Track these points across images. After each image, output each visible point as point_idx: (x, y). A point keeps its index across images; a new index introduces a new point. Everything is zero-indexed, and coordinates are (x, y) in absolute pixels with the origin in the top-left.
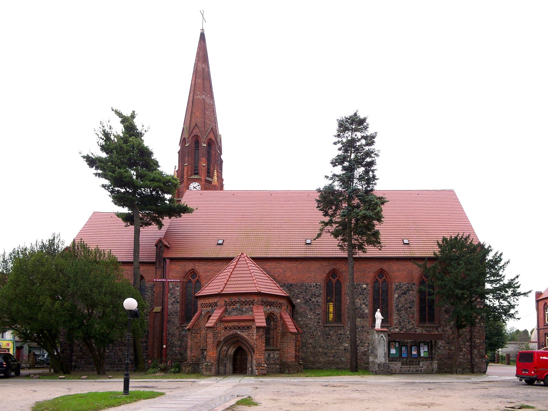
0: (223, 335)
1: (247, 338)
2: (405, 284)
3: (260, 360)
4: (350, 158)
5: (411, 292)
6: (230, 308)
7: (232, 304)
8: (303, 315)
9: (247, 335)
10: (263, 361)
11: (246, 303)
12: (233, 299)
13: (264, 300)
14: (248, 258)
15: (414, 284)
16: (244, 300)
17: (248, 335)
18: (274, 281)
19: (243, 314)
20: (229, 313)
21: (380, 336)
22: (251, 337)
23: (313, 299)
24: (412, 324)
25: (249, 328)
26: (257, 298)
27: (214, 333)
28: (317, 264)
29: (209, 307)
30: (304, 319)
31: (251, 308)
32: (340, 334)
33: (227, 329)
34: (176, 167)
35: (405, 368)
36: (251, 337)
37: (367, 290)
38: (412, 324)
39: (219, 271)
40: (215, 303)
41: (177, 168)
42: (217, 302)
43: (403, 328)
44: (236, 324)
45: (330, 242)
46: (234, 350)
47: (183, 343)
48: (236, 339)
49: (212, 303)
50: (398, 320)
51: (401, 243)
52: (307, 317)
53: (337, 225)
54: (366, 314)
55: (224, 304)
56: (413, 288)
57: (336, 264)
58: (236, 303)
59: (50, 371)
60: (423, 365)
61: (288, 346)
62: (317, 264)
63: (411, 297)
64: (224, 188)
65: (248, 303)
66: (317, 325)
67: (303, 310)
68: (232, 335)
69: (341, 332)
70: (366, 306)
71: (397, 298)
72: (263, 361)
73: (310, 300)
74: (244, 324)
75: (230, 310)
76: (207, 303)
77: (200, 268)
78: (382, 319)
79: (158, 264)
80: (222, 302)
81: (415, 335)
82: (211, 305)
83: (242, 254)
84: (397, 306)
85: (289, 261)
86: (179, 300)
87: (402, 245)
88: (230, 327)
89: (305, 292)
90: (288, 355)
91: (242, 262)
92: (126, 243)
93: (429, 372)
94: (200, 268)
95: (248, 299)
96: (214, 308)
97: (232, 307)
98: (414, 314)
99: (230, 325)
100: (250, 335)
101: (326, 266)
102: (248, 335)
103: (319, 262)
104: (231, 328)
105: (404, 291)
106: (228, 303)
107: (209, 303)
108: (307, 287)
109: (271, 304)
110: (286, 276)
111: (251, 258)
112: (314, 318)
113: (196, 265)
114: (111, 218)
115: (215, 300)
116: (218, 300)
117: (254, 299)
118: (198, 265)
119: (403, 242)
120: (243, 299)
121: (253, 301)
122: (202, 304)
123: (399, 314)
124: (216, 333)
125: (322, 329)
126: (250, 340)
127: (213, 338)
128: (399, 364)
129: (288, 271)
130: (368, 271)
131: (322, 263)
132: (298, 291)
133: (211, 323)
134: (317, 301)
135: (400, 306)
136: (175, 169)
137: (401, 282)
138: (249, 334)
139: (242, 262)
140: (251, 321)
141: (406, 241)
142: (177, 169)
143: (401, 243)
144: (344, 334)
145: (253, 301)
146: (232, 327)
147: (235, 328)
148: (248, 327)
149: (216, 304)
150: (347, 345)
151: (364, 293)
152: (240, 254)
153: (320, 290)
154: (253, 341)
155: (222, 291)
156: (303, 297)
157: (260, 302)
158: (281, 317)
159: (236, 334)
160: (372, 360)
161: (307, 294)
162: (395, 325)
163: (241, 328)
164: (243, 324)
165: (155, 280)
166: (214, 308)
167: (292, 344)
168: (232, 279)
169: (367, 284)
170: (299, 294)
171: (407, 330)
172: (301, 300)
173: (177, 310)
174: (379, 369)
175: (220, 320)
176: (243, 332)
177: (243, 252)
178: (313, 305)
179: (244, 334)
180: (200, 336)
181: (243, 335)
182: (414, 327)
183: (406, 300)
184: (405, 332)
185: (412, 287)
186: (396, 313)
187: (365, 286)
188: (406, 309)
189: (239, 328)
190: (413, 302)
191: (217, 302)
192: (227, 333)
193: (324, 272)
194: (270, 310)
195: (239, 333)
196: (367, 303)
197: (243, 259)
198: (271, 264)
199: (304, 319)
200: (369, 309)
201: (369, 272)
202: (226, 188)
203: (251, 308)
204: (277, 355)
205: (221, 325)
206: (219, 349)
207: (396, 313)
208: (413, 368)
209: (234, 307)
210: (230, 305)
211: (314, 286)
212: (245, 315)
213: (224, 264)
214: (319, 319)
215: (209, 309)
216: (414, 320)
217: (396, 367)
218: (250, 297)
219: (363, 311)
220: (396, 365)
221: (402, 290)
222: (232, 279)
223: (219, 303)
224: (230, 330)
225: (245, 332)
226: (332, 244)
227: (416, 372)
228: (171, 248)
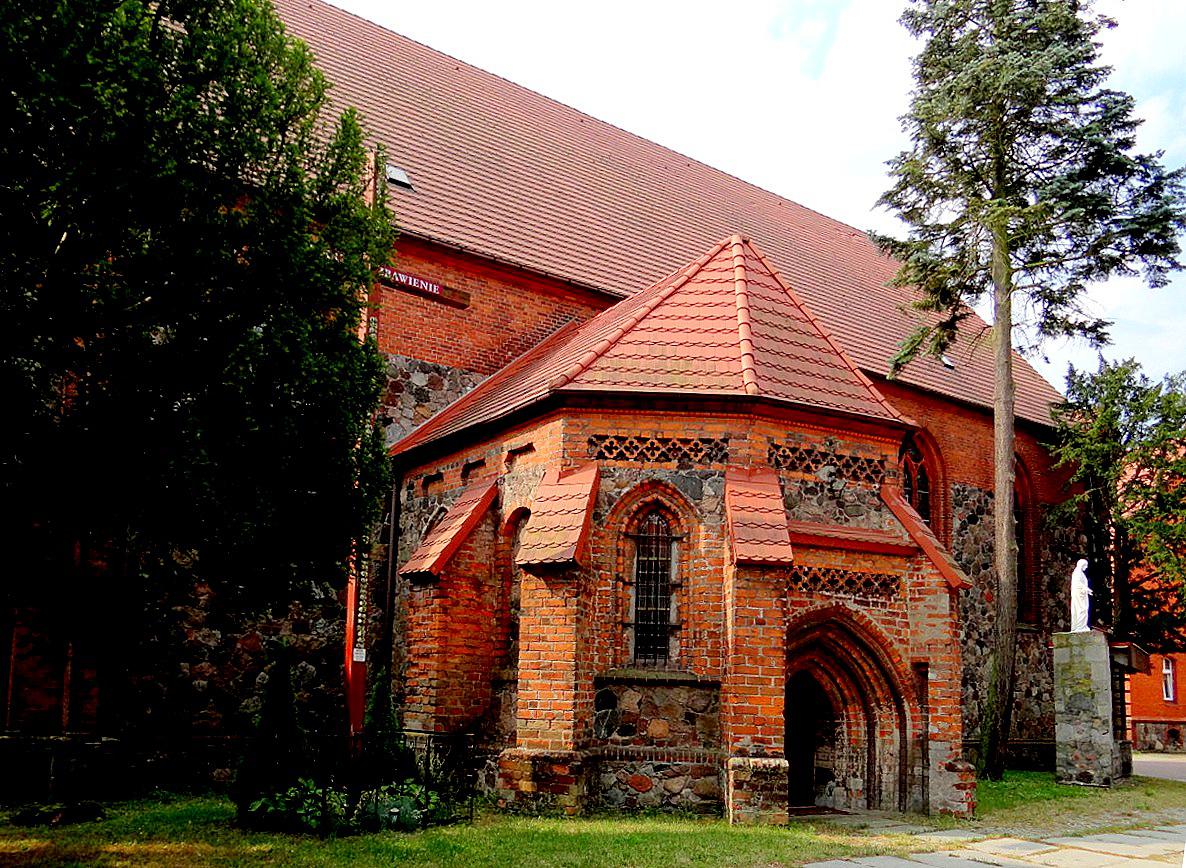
1: (885, 633)
9: (884, 622)
11: (848, 468)
16: (847, 453)
17: (889, 622)
19: (847, 520)
22: (899, 633)
33: (800, 584)
36: (899, 633)
42: (725, 440)
44: (837, 561)
47: (236, 640)
53: (1079, 194)
58: (817, 462)
59: (1128, 679)
68: (823, 613)
74: (869, 565)
76: (642, 440)
80: (762, 447)
88: (811, 575)
95: (863, 448)
96: (697, 468)
97: (799, 475)
102: (889, 622)
104: (815, 579)
105: (972, 511)
120: (844, 447)
121: (881, 463)
126: (896, 646)
140: (895, 555)
146: (820, 575)
147: (833, 582)
148: (885, 585)
155: (569, 380)
159: (840, 611)
163: (860, 584)
164: (863, 566)
166: (697, 468)
176: (868, 604)
179: (874, 616)
189: (850, 583)
192: (801, 604)
195: (852, 606)
209: (807, 476)
210: (793, 467)
212: (852, 523)
215: (665, 472)
218: (870, 444)
223: (739, 449)
224: (812, 586)
225: (875, 604)
226: (419, 223)
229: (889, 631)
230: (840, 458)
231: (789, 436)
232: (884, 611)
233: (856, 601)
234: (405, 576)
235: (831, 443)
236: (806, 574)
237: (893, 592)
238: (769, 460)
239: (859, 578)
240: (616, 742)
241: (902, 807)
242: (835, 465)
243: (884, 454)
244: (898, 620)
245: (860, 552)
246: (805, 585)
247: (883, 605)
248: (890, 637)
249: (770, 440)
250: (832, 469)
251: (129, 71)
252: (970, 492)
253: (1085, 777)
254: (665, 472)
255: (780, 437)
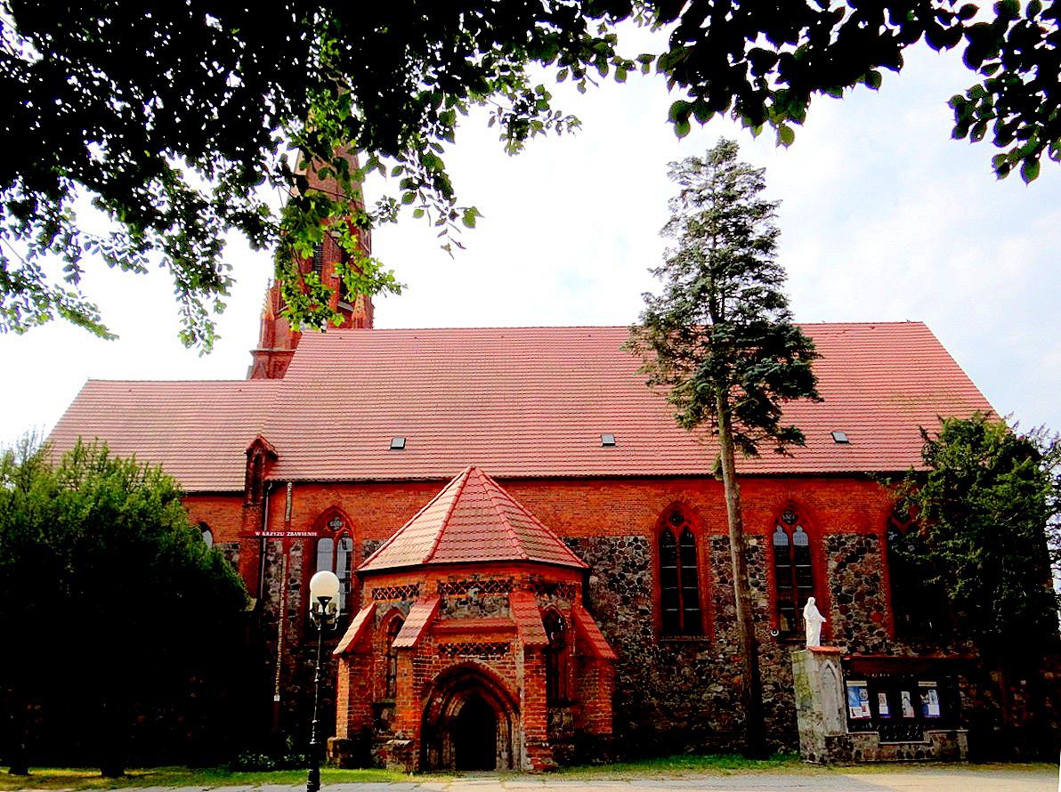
0: (434, 667)
1: (499, 674)
2: (853, 537)
3: (536, 731)
4: (89, 175)
5: (868, 556)
6: (451, 601)
7: (457, 589)
8: (606, 614)
9: (498, 668)
10: (542, 733)
11: (491, 587)
12: (461, 578)
13: (536, 579)
14: (486, 478)
15: (874, 537)
16: (487, 580)
18: (550, 532)
19: (486, 615)
20: (449, 612)
21: (825, 665)
22: (509, 673)
23: (628, 576)
24: (880, 634)
25: (502, 649)
26: (519, 574)
27: (416, 661)
28: (634, 493)
29: (397, 597)
30: (609, 625)
31: (504, 599)
32: (701, 662)
34: (270, 280)
35: (892, 747)
37: (760, 551)
38: (880, 634)
39: (414, 510)
40: (411, 586)
41: (272, 285)
42: (418, 585)
43: (856, 644)
44: (469, 639)
45: (578, 428)
46: (461, 707)
48: (468, 676)
49: (404, 587)
50: (843, 624)
51: (829, 441)
52: (617, 619)
54: (761, 610)
55: (436, 589)
56: (872, 546)
57: (681, 491)
58: (468, 587)
60: (932, 740)
61: (595, 693)
62: (634, 491)
63: (870, 568)
64: (374, 324)
65: (497, 586)
66: (642, 640)
67: (606, 601)
69: (703, 656)
70: (761, 589)
71: (836, 571)
72: (542, 733)
73: (623, 577)
74: (489, 638)
75: (451, 604)
76: (390, 589)
77: (353, 505)
78: (823, 623)
79: (250, 496)
81: (889, 662)
82: (400, 593)
83: (473, 469)
84: (838, 588)
85: (566, 486)
86: (298, 582)
87: (832, 446)
89: (610, 559)
90: (598, 717)
91: (475, 489)
92: (377, 466)
93: (947, 758)
94: (353, 505)
97: (456, 596)
98: (881, 608)
99: (455, 641)
100: (505, 668)
101: (657, 495)
102: (502, 668)
103: (638, 488)
105: (851, 552)
106: (447, 588)
107: (397, 588)
108: (612, 545)
109: (550, 589)
110: (562, 521)
111: (495, 478)
112: (635, 622)
113: (344, 496)
114: (130, 393)
115: (414, 580)
116: (422, 580)
117: (513, 578)
118: (348, 496)
119: (834, 438)
120: (483, 577)
121: (510, 581)
122: (376, 590)
123: (844, 611)
124: (421, 661)
125: (655, 649)
126: (506, 680)
127: (415, 675)
128: (875, 738)
129: (565, 508)
130: (758, 506)
131: (648, 488)
132: (593, 555)
133: (404, 640)
134: (640, 580)
135: (844, 589)
136: (269, 285)
137: (840, 533)
138: (503, 663)
139: (475, 489)
140: (506, 632)
141: (840, 437)
142: (272, 286)
143: (829, 441)
144: (710, 662)
145: (510, 581)
149: (415, 591)
150: (720, 688)
151: (754, 558)
152: (467, 470)
153: (644, 553)
154: (514, 682)
156: (606, 571)
157: (527, 582)
158: (574, 619)
159: (471, 663)
160: (807, 727)
161: (614, 564)
162: (838, 637)
164: (487, 639)
165: (257, 534)
166: (408, 599)
167: (604, 689)
168: (453, 529)
169: (758, 538)
170: (594, 564)
171: (867, 648)
172: (600, 578)
173: (295, 606)
174: (830, 750)
175: (430, 629)
176: (487, 659)
177: (477, 465)
178: (631, 590)
179: (491, 665)
180: (372, 671)
181: (487, 666)
182: (884, 640)
183: (857, 575)
184: (863, 653)
185: (868, 543)
186: (836, 608)
187: (753, 542)
188: (860, 597)
190: (876, 578)
191: (418, 585)
192: (448, 663)
193: (655, 511)
194: (549, 604)
195: (477, 661)
196: (762, 584)
197: (476, 482)
198: (523, 494)
199: (609, 625)
200: (768, 598)
201: (762, 508)
202: (377, 324)
203: (504, 599)
204: (568, 718)
205: (430, 640)
206: (426, 700)
207: (836, 608)
208: (907, 747)
209: (460, 596)
210: (451, 593)
211: (630, 544)
212: (489, 616)
213: (411, 493)
214: (647, 623)
215: (397, 603)
216: (884, 625)
217: (868, 744)
219: (756, 604)
220: (866, 739)
221: (845, 550)
222: (453, 529)
223: (422, 589)
225: (493, 659)
227: (916, 757)
228: (282, 459)
229: (503, 673)
230: (482, 583)
231: (450, 577)
232: (499, 661)
233: (480, 658)
234: (394, 648)
235: (476, 577)
236: (449, 647)
237: (506, 651)
238: (438, 591)
239: (483, 646)
240: (380, 734)
241: (510, 766)
242: (479, 587)
243: (512, 575)
244: (508, 666)
245: (482, 633)
246: (449, 653)
247: (499, 659)
248: (502, 676)
249: (439, 581)
250: (477, 589)
251: (1049, 142)
252: (846, 539)
253: (812, 757)
254: (397, 603)
255: (444, 579)
